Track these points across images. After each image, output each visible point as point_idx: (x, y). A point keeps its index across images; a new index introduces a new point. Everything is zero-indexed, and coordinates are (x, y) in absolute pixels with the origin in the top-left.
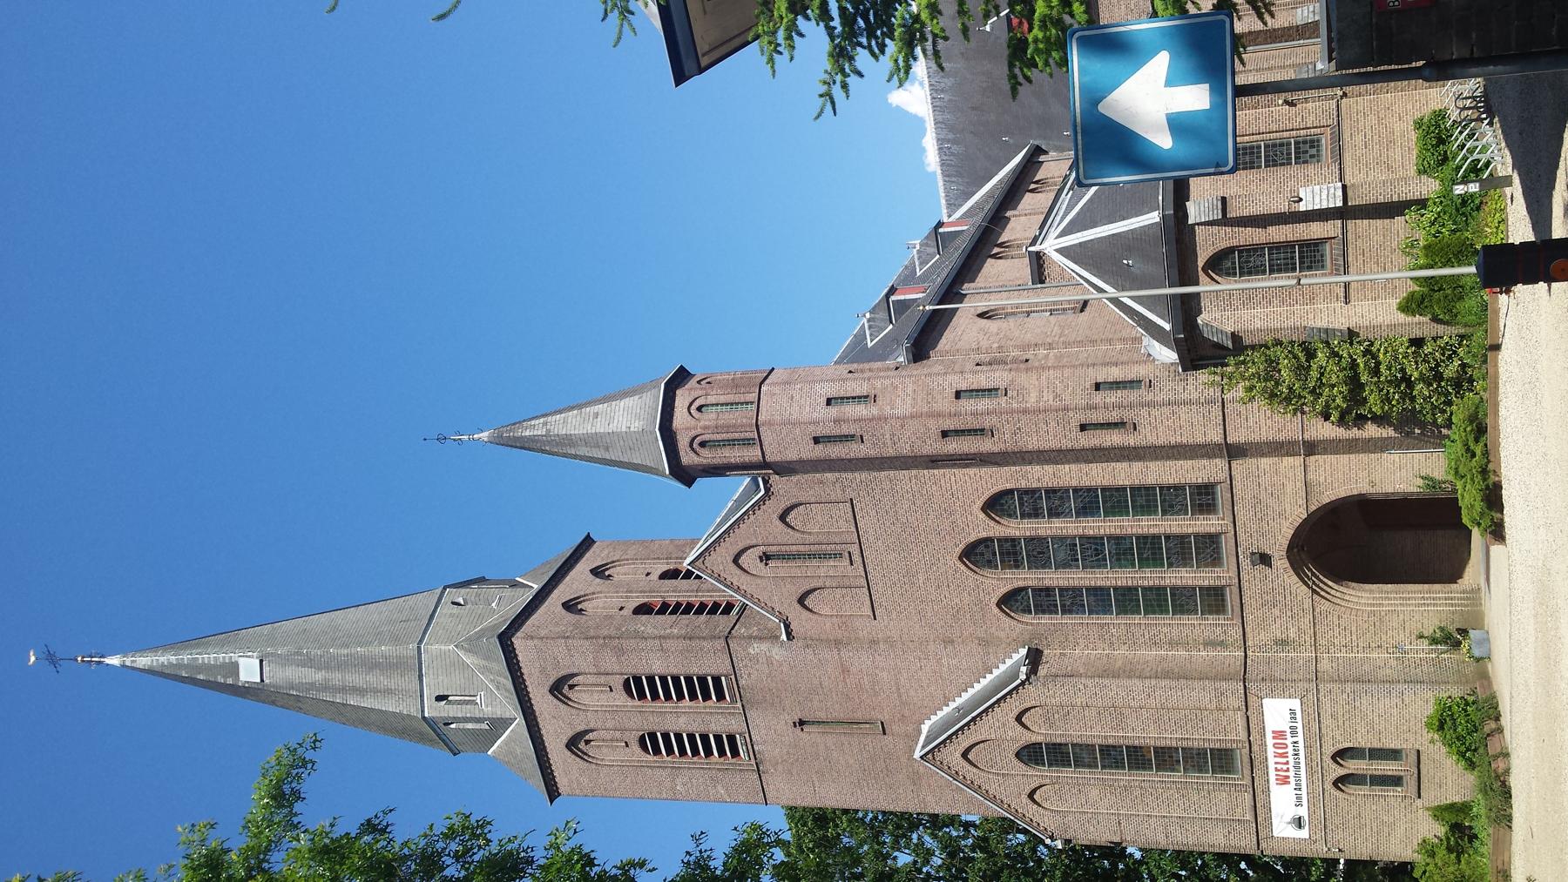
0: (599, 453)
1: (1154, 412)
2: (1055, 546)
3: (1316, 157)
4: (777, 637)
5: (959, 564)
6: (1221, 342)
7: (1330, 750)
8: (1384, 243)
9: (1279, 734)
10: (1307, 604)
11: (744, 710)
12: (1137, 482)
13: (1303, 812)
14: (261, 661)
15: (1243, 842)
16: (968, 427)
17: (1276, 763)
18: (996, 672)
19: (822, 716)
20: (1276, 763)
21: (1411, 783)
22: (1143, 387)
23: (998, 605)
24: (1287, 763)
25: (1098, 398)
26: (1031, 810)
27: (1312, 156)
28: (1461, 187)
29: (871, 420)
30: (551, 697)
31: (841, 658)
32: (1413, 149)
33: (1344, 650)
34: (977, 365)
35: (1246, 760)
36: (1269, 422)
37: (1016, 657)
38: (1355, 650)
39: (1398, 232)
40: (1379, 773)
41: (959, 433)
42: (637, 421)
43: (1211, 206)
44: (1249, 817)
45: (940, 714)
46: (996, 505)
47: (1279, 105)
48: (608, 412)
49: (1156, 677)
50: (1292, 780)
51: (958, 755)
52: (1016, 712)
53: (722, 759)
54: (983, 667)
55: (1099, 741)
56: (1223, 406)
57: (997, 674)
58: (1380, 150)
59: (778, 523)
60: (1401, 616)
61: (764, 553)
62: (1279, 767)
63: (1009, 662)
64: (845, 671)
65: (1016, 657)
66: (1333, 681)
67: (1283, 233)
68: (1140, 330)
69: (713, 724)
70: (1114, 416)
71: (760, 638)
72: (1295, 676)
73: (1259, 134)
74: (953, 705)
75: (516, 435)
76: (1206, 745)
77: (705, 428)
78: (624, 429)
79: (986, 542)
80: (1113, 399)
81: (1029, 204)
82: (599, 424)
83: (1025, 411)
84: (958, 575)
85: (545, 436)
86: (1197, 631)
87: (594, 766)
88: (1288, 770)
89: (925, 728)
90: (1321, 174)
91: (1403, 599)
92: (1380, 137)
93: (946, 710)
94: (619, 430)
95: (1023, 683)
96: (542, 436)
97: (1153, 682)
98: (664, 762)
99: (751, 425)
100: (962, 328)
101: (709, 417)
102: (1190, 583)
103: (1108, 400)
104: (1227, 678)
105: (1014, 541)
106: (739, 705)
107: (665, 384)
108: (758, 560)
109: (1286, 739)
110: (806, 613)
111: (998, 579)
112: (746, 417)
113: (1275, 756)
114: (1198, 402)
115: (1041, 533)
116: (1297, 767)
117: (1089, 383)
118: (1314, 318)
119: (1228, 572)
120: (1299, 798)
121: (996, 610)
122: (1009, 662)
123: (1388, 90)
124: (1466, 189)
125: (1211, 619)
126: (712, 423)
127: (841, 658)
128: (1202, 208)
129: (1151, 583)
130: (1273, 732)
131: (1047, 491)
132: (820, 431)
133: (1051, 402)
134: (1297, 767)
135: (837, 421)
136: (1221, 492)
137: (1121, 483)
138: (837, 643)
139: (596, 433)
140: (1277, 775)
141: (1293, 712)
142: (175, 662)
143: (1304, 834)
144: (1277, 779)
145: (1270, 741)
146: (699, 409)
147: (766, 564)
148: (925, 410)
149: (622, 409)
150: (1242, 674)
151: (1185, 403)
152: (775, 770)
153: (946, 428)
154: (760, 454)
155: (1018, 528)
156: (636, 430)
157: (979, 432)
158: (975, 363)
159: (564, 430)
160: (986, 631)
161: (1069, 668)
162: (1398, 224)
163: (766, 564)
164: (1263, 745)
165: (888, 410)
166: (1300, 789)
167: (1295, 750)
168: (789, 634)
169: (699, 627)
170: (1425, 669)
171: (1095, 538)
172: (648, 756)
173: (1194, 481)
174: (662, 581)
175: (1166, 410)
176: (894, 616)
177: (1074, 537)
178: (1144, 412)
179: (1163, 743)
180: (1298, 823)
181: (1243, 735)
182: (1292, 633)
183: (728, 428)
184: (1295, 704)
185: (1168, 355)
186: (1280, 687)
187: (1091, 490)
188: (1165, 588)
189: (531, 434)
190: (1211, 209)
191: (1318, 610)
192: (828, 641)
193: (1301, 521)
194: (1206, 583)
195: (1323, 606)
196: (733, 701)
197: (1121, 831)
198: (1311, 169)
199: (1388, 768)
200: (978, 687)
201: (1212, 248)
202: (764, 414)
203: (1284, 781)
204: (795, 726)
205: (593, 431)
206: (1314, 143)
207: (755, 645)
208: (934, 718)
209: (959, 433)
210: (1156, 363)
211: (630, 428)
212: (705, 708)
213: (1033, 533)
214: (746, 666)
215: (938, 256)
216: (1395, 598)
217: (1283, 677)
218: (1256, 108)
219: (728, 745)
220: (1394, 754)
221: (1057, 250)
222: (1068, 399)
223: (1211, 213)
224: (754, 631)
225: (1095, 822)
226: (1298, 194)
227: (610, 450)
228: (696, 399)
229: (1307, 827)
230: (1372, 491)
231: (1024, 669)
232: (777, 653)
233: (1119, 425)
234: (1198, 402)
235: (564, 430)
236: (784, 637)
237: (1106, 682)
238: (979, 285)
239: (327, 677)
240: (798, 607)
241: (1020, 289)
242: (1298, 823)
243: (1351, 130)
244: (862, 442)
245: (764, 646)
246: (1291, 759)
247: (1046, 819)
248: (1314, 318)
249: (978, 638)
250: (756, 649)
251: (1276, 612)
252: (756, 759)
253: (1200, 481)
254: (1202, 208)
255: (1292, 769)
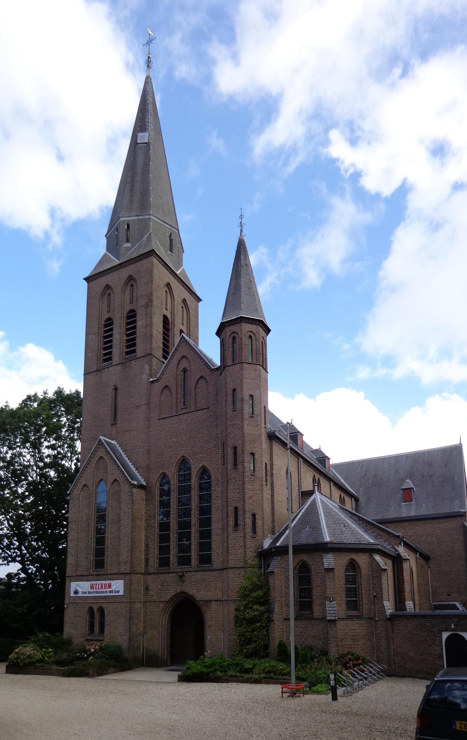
0: (232, 290)
1: (242, 539)
2: (187, 497)
3: (349, 608)
4: (151, 377)
5: (181, 456)
6: (270, 567)
7: (104, 606)
8: (310, 636)
9: (110, 586)
10: (163, 599)
11: (121, 363)
12: (213, 532)
13: (80, 595)
14: (146, 143)
15: (69, 571)
16: (238, 458)
17: (99, 584)
18: (136, 472)
19: (119, 398)
20: (99, 584)
21: (90, 638)
22: (253, 534)
23: (163, 473)
24: (99, 589)
25: (248, 516)
26: (80, 486)
27: (350, 607)
28: (333, 677)
29: (242, 415)
30: (128, 276)
31: (143, 405)
32: (350, 649)
33: (144, 613)
34: (251, 396)
35: (100, 573)
36: (236, 586)
37: (142, 480)
38: (144, 617)
39: (314, 642)
40: (95, 625)
41: (235, 454)
42: (246, 307)
43: (330, 563)
44: (79, 573)
45: (119, 449)
46: (204, 471)
47: (373, 593)
48: (251, 294)
49: (132, 538)
50: (92, 590)
51: (102, 455)
52: (118, 479)
53: (102, 355)
54: (139, 466)
55: (107, 514)
56: (243, 568)
57: (142, 481)
58: (351, 636)
59: (200, 376)
60: (157, 636)
61: (187, 370)
62: (97, 585)
63: (140, 478)
64: (137, 407)
65: (142, 480)
66: (131, 608)
67: (317, 594)
68: (278, 534)
69: (116, 350)
70: (240, 522)
71: (151, 369)
72: (132, 593)
73: (361, 585)
74: (123, 454)
75: (242, 251)
76: (106, 557)
77: (241, 339)
78: (242, 301)
79: (189, 469)
80: (248, 521)
81: (335, 494)
82: (245, 290)
83: (244, 484)
84: (176, 456)
85: (241, 265)
86: (152, 555)
87: (99, 298)
88: (96, 589)
89: (114, 442)
90: (342, 611)
91: (164, 637)
92: (357, 635)
93: (121, 451)
94: (242, 299)
95: (130, 482)
96: (241, 264)
97: (130, 536)
98: (101, 329)
99: (241, 360)
100: (283, 459)
101: (246, 341)
102: (172, 552)
103: (248, 519)
104: (132, 567)
105: (190, 480)
106: (124, 361)
107: (262, 320)
108: (184, 368)
109: (108, 589)
110: (161, 389)
111: (174, 473)
112: (246, 358)
113: (101, 584)
114: (245, 557)
115: (193, 492)
116: (97, 592)
117: (256, 511)
118: (278, 606)
119: (176, 568)
120: (85, 593)
121: (161, 472)
122: (140, 478)
123: (377, 639)
124: (332, 679)
125: (157, 561)
126: (243, 342)
127: (143, 405)
128: (329, 560)
129: (171, 537)
130: (111, 584)
131: (210, 494)
132: (238, 391)
133: (248, 495)
134: (97, 592)
135: (242, 399)
136: (208, 566)
137: (213, 525)
138: (149, 404)
139: (241, 288)
140: (94, 584)
141: (118, 592)
142: (147, 102)
143: (72, 594)
144: (92, 584)
145: (107, 582)
146: (250, 337)
147: (182, 371)
148: (246, 439)
149: (251, 300)
150: (134, 572)
151: (245, 552)
152: (98, 378)
153: (238, 449)
154: (229, 365)
155: (194, 482)
156: (242, 306)
157: (235, 465)
158: (266, 463)
159: (243, 274)
160: (153, 468)
161: (136, 502)
162: (318, 642)
163: (182, 371)
164: (105, 580)
165: (246, 422)
166: (89, 593)
167: (104, 592)
168: (152, 382)
169: (157, 343)
170: (136, 644)
171: (190, 514)
172: (103, 323)
173: (213, 555)
174: (179, 330)
175: (242, 544)
176: (160, 428)
177: (190, 505)
178: (242, 534)
179: (106, 540)
180: (76, 592)
181: (110, 572)
182: (151, 593)
183: (241, 349)
184: (121, 593)
185: (267, 544)
186: (127, 587)
187: (210, 513)
188: (169, 542)
189: (242, 259)
190: (329, 563)
191: (160, 603)
192: (149, 399)
193: (196, 598)
194: (171, 559)
195: (162, 606)
196: (125, 359)
197: (72, 522)
198: (344, 606)
199: (97, 629)
200: (130, 464)
201: (312, 564)
202: (247, 366)
203: (92, 587)
204: (115, 386)
205: (242, 287)
206: (356, 608)
207: (148, 367)
208: (118, 446)
209: (235, 454)
210: (263, 540)
211: (243, 303)
212: (123, 346)
213: (193, 488)
214: (139, 363)
215: (316, 458)
216: (165, 633)
217: (132, 588)
218: (372, 584)
219: (108, 358)
220: (102, 631)
221: (315, 498)
222: (248, 502)
223: (327, 563)
224: (154, 367)
225: (76, 512)
226: (333, 601)
227: (234, 295)
228: (255, 335)
229: (75, 595)
230: (207, 626)
231: (136, 483)
232: (145, 377)
233: (236, 524)
234: (245, 557)
235: (243, 274)
236: (151, 380)
237: (130, 518)
238: (302, 466)
239: (139, 174)
240: (164, 386)
241: (299, 486)
242: (76, 592)
243: (360, 623)
244: (233, 411)
245: (147, 371)
246: (100, 590)
247: (76, 491)
248: (278, 606)
249: (150, 464)
250: (147, 368)
251: (159, 587)
252: (102, 369)
253: (213, 557)
254: (329, 560)
255: (96, 590)
